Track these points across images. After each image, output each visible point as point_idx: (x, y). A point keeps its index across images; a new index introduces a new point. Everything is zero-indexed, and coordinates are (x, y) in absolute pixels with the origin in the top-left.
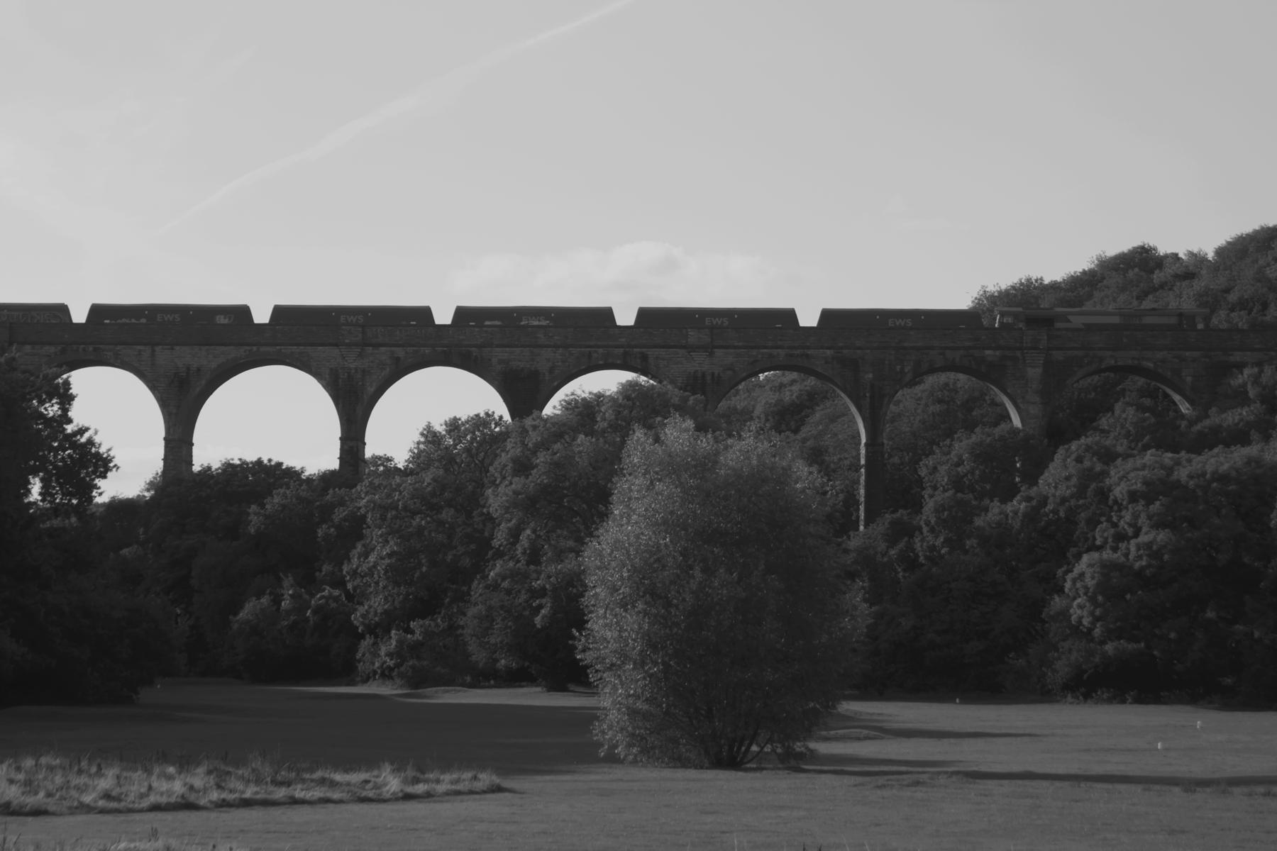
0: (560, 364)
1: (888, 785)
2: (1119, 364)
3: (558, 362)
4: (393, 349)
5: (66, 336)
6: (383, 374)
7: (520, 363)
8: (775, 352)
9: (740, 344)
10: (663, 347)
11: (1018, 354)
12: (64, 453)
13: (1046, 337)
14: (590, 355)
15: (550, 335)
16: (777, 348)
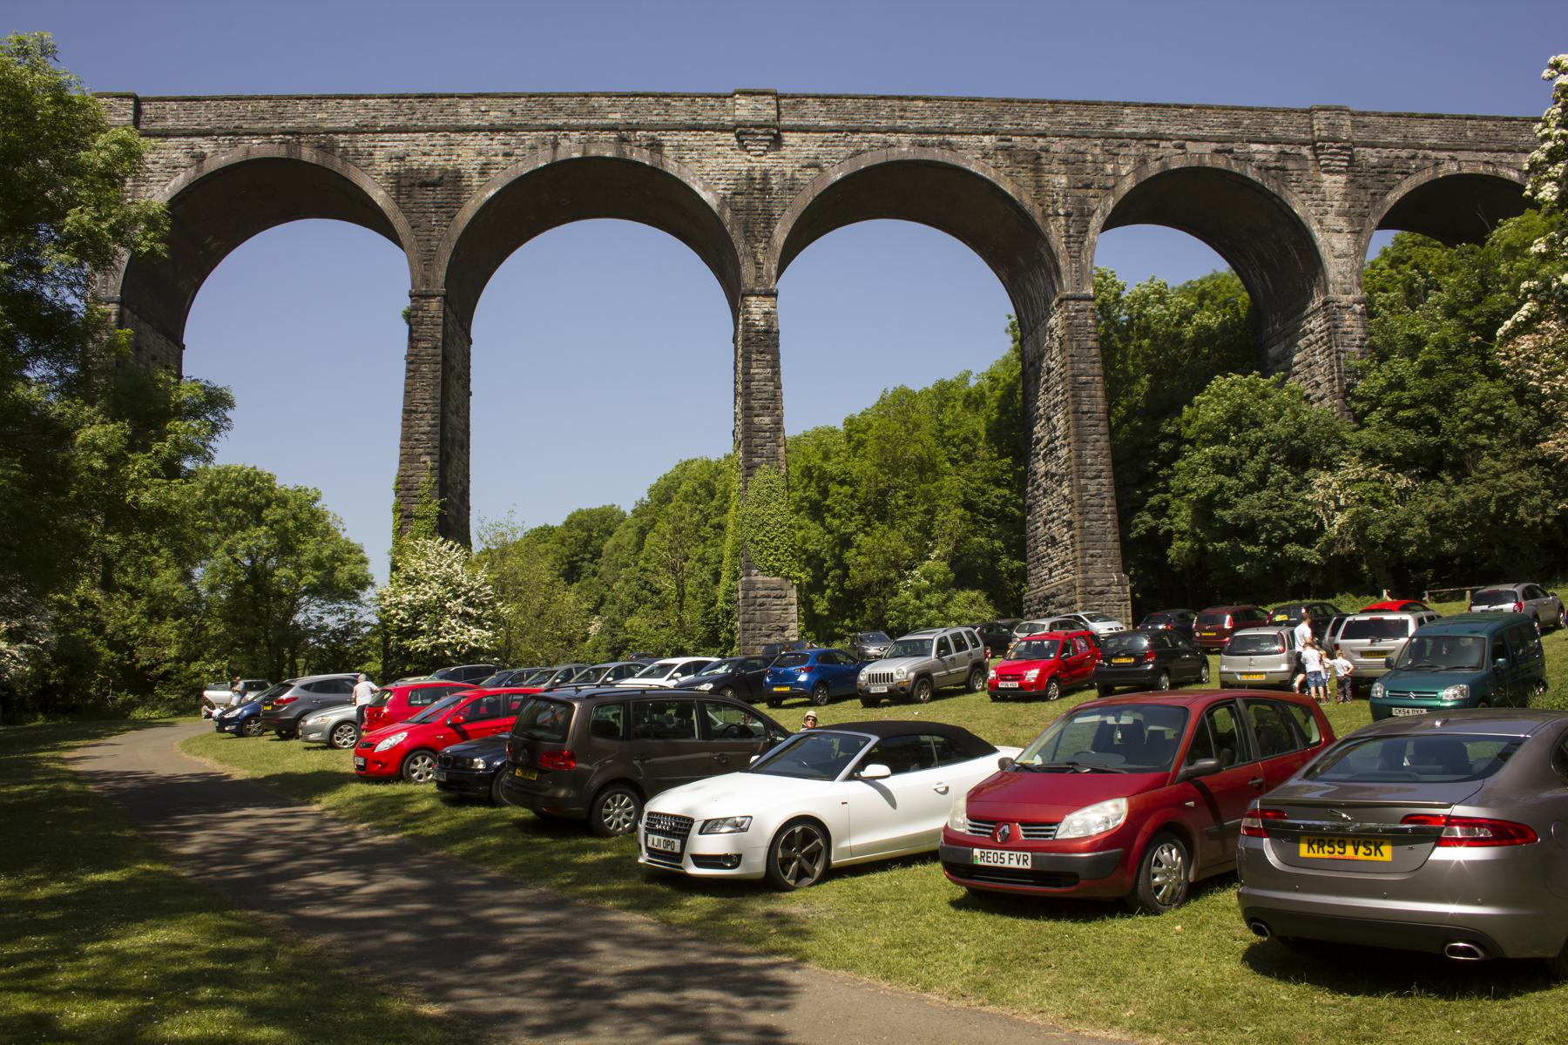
0: (500, 158)
1: (885, 132)
2: (1465, 171)
3: (496, 155)
4: (191, 140)
5: (1438, 724)
6: (172, 184)
7: (425, 158)
8: (893, 138)
9: (831, 123)
10: (689, 128)
11: (1305, 151)
12: (1236, 628)
13: (1349, 123)
14: (555, 145)
15: (483, 108)
16: (896, 131)
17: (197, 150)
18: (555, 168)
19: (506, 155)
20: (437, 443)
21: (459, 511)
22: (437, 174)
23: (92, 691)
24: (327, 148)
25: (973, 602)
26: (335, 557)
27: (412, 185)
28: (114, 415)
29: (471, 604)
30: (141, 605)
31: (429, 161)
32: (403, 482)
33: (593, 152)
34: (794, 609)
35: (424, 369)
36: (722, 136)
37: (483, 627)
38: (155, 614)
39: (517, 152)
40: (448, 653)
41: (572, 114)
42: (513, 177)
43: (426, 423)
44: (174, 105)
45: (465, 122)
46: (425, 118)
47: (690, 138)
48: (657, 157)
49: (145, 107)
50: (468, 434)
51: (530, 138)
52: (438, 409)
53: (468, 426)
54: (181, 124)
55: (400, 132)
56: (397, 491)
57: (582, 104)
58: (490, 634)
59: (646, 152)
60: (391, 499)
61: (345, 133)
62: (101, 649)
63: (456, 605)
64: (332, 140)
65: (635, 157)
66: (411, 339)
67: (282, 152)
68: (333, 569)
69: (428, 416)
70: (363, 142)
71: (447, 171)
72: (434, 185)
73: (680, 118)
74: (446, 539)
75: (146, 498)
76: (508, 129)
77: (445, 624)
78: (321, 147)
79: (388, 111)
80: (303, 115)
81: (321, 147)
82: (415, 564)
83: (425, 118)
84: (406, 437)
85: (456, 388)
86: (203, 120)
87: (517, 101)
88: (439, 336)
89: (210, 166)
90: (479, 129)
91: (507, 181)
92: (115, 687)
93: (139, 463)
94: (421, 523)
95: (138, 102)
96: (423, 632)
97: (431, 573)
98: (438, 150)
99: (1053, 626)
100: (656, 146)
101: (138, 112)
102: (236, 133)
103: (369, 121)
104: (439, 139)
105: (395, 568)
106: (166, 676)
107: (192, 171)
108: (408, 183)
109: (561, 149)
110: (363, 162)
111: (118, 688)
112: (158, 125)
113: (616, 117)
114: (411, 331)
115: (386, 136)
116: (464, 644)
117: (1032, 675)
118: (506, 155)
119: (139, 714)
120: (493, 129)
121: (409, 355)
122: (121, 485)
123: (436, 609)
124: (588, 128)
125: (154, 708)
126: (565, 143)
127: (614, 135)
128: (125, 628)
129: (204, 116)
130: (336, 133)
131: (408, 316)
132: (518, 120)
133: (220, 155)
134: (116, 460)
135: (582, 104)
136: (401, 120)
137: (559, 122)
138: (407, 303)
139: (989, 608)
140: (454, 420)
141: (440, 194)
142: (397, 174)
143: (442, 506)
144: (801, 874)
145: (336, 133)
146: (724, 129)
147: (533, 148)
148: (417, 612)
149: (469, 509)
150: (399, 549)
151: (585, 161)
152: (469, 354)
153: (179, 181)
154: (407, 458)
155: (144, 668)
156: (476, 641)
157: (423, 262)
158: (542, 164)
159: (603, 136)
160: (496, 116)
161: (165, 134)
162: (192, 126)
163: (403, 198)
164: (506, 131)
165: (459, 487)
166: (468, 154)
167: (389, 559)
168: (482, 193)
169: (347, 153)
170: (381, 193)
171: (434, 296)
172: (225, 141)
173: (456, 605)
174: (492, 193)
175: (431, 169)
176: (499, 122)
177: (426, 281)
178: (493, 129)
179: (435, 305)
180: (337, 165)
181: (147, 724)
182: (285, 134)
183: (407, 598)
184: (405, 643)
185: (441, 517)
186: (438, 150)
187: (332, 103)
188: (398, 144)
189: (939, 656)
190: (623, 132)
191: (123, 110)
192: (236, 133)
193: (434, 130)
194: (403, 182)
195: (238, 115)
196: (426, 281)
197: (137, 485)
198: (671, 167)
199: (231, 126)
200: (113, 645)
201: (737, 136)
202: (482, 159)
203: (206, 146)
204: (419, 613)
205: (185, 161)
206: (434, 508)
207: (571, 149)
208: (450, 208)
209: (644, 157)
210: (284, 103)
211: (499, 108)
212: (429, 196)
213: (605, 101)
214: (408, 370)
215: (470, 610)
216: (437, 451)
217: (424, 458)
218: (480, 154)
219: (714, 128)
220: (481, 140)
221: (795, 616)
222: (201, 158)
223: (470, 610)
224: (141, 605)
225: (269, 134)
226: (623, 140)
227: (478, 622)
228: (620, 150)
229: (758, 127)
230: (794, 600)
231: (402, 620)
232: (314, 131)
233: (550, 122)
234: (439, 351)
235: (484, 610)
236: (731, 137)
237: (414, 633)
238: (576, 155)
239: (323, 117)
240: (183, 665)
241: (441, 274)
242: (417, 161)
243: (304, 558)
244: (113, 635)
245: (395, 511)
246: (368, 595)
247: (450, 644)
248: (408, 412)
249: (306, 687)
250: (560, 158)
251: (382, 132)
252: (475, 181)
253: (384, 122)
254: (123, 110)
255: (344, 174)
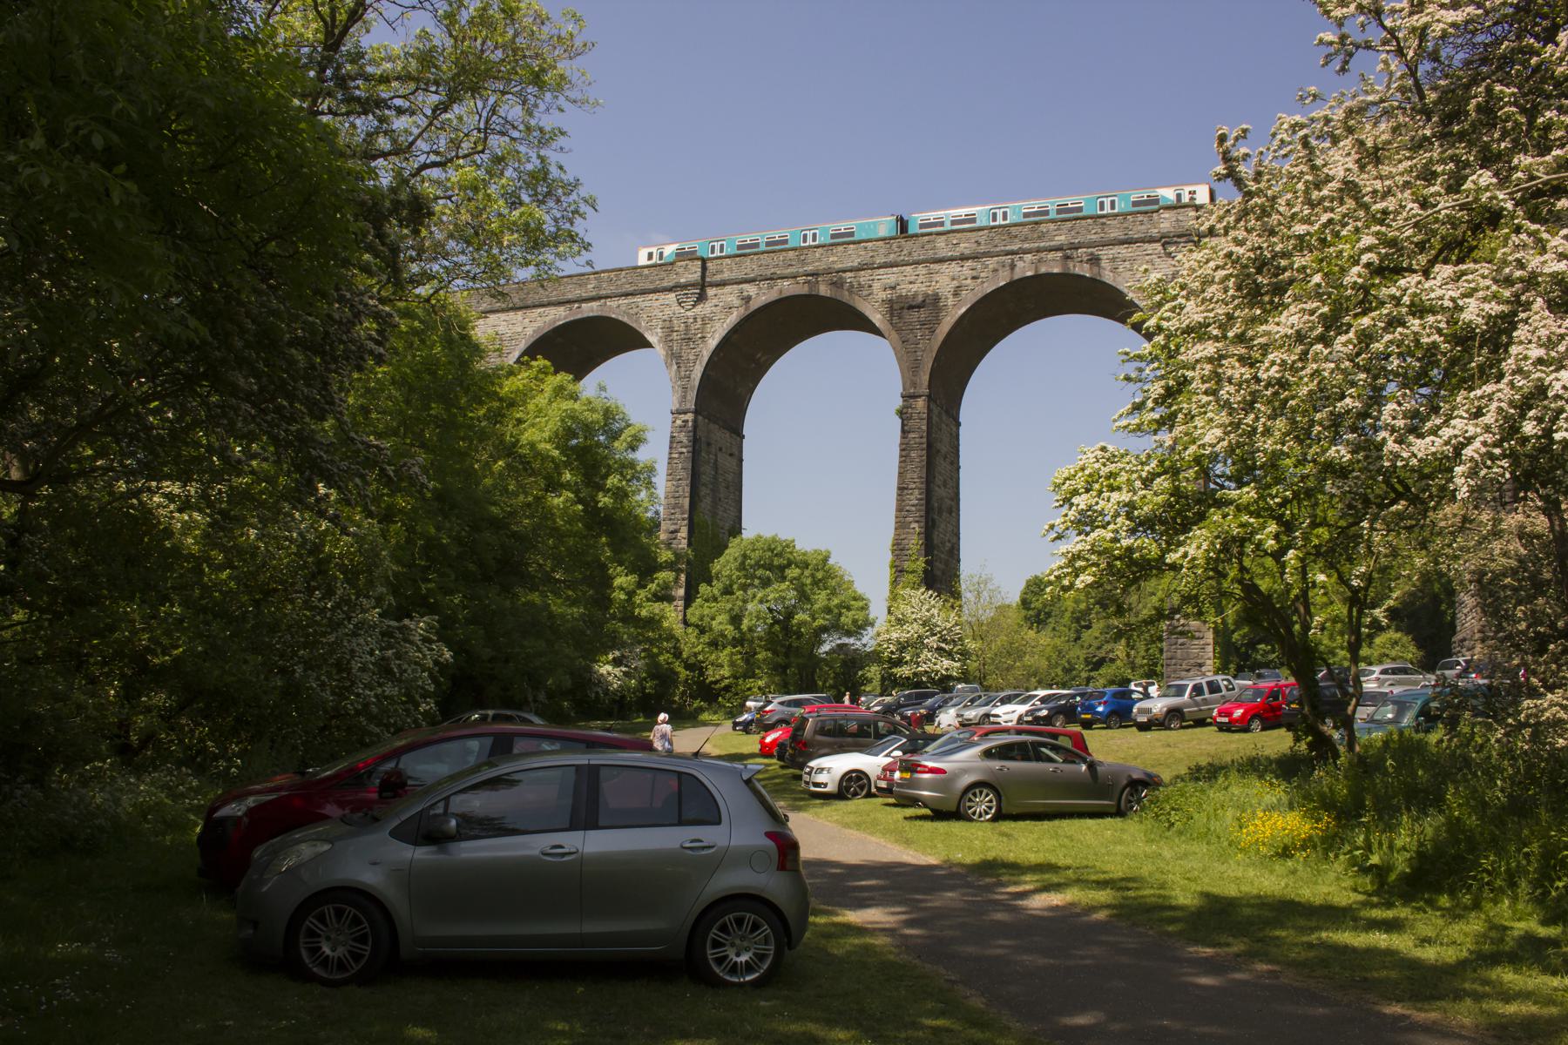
0: (969, 281)
10: (1122, 242)
14: (1013, 267)
17: (745, 294)
18: (1013, 285)
19: (974, 278)
20: (923, 513)
21: (947, 563)
22: (920, 298)
23: (677, 698)
24: (837, 284)
25: (1396, 643)
26: (842, 606)
27: (902, 308)
28: (631, 572)
29: (945, 641)
30: (706, 638)
31: (914, 288)
32: (898, 544)
33: (1043, 270)
34: (1210, 648)
35: (913, 454)
36: (1150, 247)
37: (953, 660)
38: (714, 644)
39: (982, 275)
40: (924, 679)
41: (1026, 240)
42: (980, 295)
43: (915, 497)
44: (728, 261)
45: (942, 254)
46: (910, 254)
47: (1123, 251)
48: (1095, 269)
49: (709, 265)
50: (958, 500)
51: (992, 262)
52: (924, 486)
53: (957, 494)
54: (733, 276)
55: (892, 266)
56: (893, 551)
57: (1033, 230)
58: (958, 664)
59: (1086, 266)
60: (889, 557)
61: (851, 271)
62: (679, 669)
63: (932, 641)
64: (841, 278)
65: (1077, 271)
66: (903, 431)
67: (805, 290)
68: (840, 614)
69: (916, 492)
70: (864, 276)
71: (928, 295)
72: (919, 307)
73: (1115, 234)
74: (928, 589)
75: (644, 613)
76: (975, 257)
77: (923, 656)
78: (833, 284)
79: (882, 251)
80: (819, 260)
81: (833, 284)
82: (904, 609)
83: (910, 254)
84: (900, 509)
85: (942, 466)
86: (748, 270)
87: (981, 233)
88: (924, 428)
89: (755, 305)
90: (952, 259)
91: (975, 299)
92: (691, 696)
93: (642, 594)
94: (911, 576)
95: (704, 261)
96: (906, 663)
97: (914, 616)
98: (921, 278)
99: (1383, 672)
100: (1094, 261)
101: (704, 268)
102: (772, 278)
103: (868, 260)
104: (921, 269)
105: (889, 612)
106: (727, 688)
107: (742, 310)
108: (900, 308)
109: (1017, 269)
110: (865, 293)
111: (693, 697)
112: (718, 278)
113: (1061, 239)
114: (903, 425)
115: (881, 271)
116: (937, 672)
117: (1238, 713)
118: (974, 278)
119: (705, 716)
120: (963, 258)
121: (901, 444)
122: (633, 605)
123: (917, 644)
124: (1039, 250)
125: (715, 713)
126: (1020, 264)
127: (1060, 254)
128: (695, 655)
129: (749, 267)
130: (844, 271)
131: (901, 413)
132: (982, 249)
133: (761, 295)
134: (631, 594)
135: (1033, 230)
136: (892, 257)
137: (1015, 248)
138: (899, 402)
139: (1412, 648)
140: (940, 492)
141: (923, 314)
142: (891, 300)
143: (927, 562)
144: (855, 794)
145: (844, 271)
146: (1152, 240)
147: (995, 270)
148: (903, 647)
149: (959, 561)
150: (894, 597)
151: (1037, 277)
152: (958, 435)
153: (733, 318)
154: (901, 525)
155: (712, 683)
156: (947, 669)
157: (910, 368)
158: (1002, 284)
159: (1051, 255)
160: (965, 247)
161: (723, 284)
162: (741, 276)
163: (895, 320)
164: (974, 258)
165: (948, 544)
166: (944, 280)
167: (886, 604)
168: (955, 311)
169: (852, 286)
170: (879, 316)
171: (920, 396)
172: (763, 285)
173: (932, 641)
174: (963, 310)
175: (915, 295)
176: (967, 252)
177: (914, 385)
178: (963, 258)
179: (921, 404)
180: (845, 297)
181: (705, 724)
182: (807, 275)
183: (895, 635)
184: (895, 670)
185: (925, 571)
186: (921, 278)
187: (840, 248)
188: (890, 277)
189: (1191, 697)
190: (1067, 251)
191: (694, 269)
192: (772, 278)
193: (917, 263)
194: (895, 306)
195: (773, 264)
196: (914, 385)
197: (640, 606)
198: (1108, 277)
199: (769, 273)
200: (688, 667)
201: (1163, 245)
202: (955, 283)
203: (751, 289)
204: (904, 648)
205: (737, 302)
206: (920, 564)
207: (1025, 268)
208: (931, 325)
209: (1084, 270)
210: (805, 252)
211: (968, 240)
212: (914, 316)
213: (1052, 226)
214: (901, 456)
215: (943, 645)
216: (923, 519)
217: (913, 525)
218: (953, 279)
219: (1143, 241)
220: (954, 268)
221: (1211, 655)
222: (748, 299)
223: (943, 645)
224: (706, 638)
225: (795, 277)
226: (1067, 258)
227: (950, 655)
228: (1065, 266)
229: (1179, 236)
230: (1211, 641)
231: (892, 653)
232: (828, 272)
233: (1008, 248)
234: (925, 440)
235: (955, 645)
236: (1158, 246)
237: (899, 662)
238: (1029, 274)
239: (837, 259)
240: (741, 681)
241: (925, 378)
242: (905, 289)
243: (816, 607)
244: (688, 658)
245: (892, 567)
246: (871, 631)
247: (926, 672)
248: (902, 489)
249: (782, 703)
250: (1016, 277)
251: (879, 268)
252: (950, 302)
253: (879, 260)
254: (694, 269)
255: (851, 303)
